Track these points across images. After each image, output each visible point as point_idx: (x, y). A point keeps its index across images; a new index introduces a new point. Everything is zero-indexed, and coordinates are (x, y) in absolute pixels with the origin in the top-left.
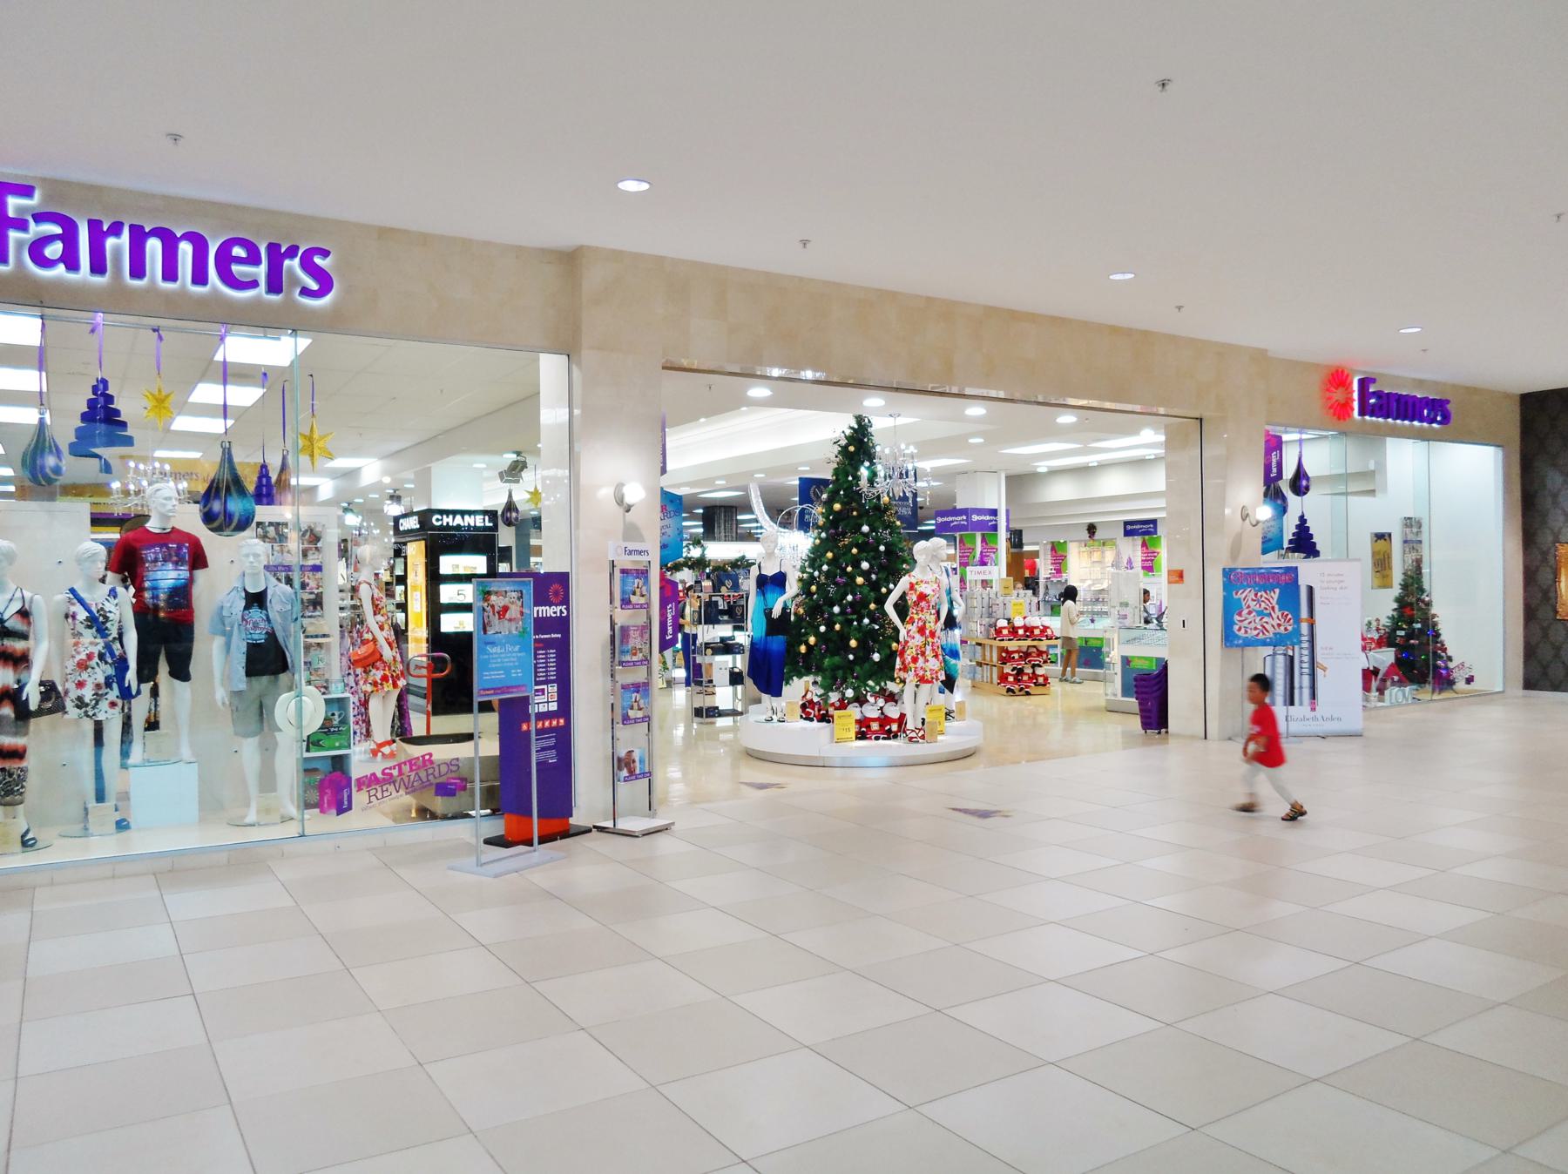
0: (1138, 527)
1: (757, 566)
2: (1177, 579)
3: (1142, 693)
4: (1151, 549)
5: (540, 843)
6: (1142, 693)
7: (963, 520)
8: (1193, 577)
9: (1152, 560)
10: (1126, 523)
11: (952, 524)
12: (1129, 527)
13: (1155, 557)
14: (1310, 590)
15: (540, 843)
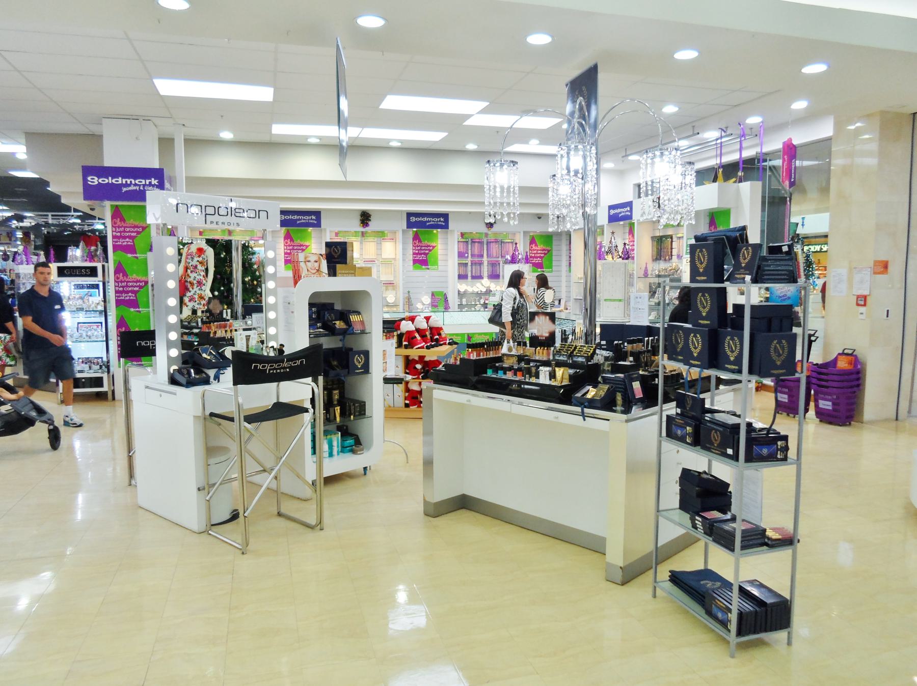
0: (426, 219)
1: (9, 242)
2: (882, 270)
3: (761, 629)
4: (425, 242)
5: (743, 548)
6: (761, 629)
7: (627, 211)
8: (896, 269)
9: (426, 254)
10: (409, 215)
11: (620, 215)
12: (413, 219)
13: (430, 250)
14: (120, 367)
15: (743, 548)
